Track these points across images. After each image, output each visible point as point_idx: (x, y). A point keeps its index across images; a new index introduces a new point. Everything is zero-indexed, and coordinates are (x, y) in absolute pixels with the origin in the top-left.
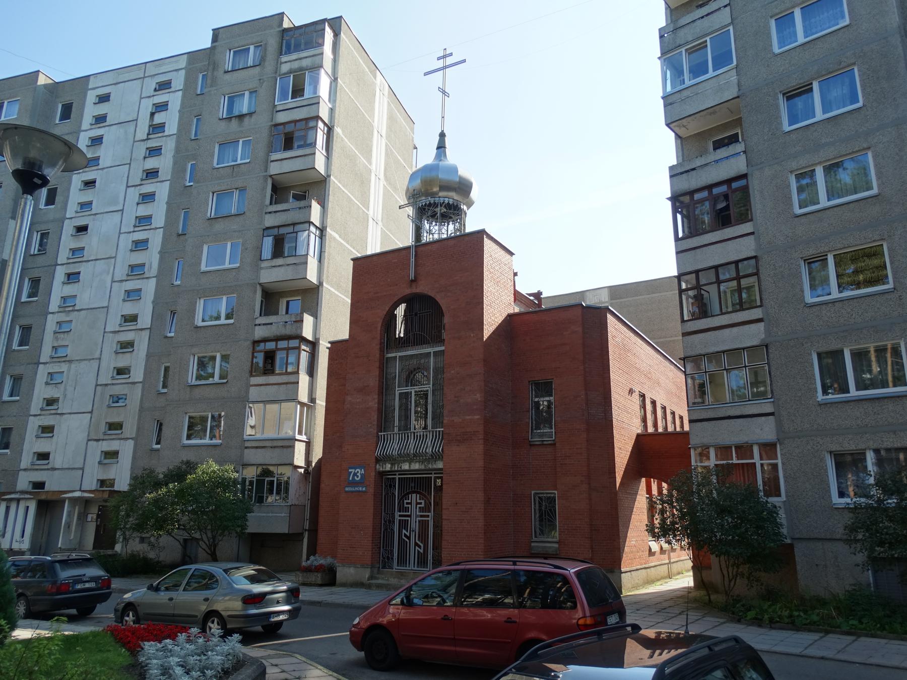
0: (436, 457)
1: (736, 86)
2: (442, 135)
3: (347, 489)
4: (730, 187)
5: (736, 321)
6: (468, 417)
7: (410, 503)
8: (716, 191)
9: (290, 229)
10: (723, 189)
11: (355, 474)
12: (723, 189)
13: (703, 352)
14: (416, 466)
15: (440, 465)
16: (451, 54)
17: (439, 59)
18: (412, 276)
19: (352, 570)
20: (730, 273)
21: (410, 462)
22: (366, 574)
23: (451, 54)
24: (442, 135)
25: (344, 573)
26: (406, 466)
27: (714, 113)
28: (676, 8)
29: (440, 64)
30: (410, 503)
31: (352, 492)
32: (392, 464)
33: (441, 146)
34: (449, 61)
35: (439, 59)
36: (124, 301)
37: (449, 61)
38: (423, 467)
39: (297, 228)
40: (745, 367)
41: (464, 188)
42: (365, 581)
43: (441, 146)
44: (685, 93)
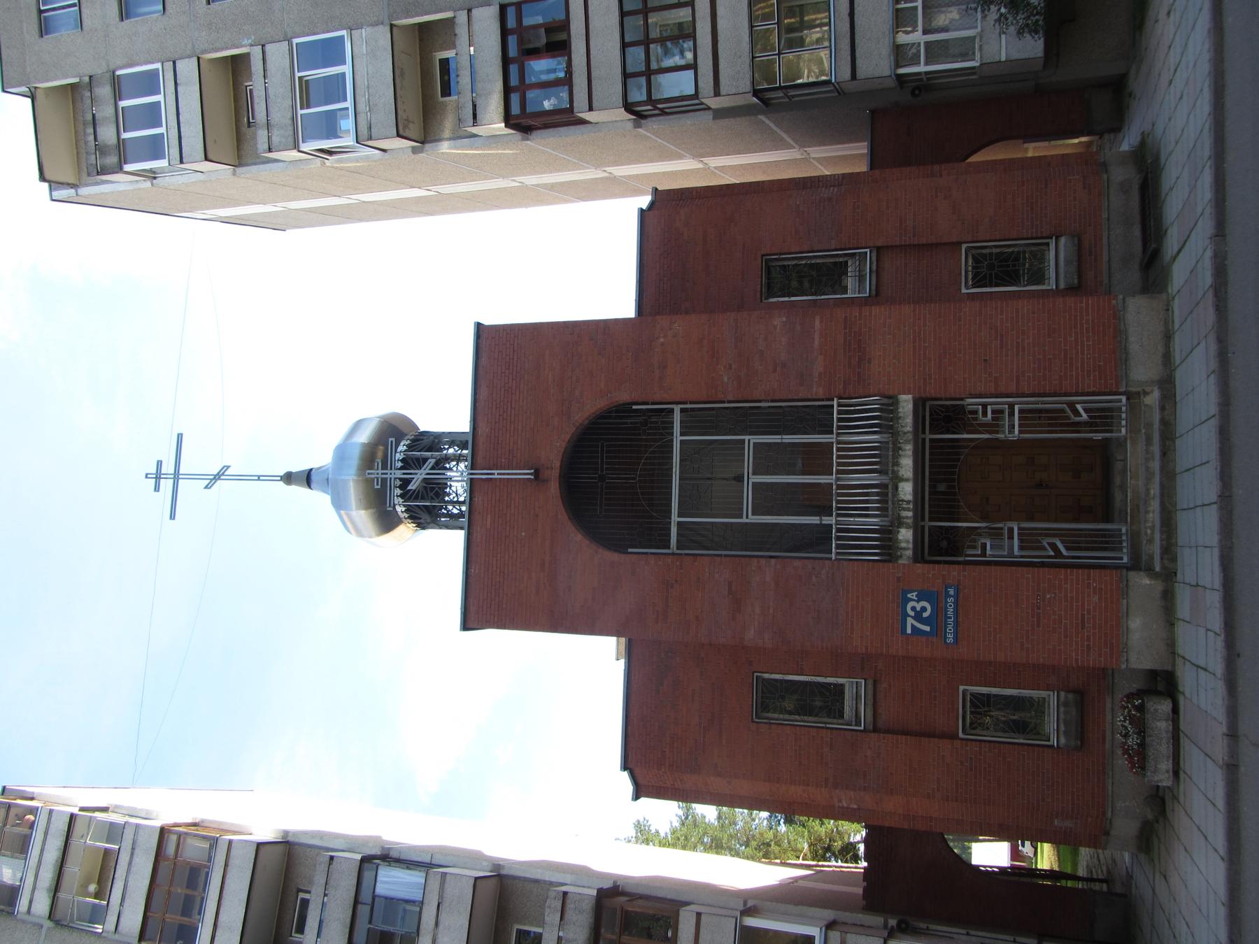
0: (887, 419)
1: (376, 28)
2: (289, 478)
3: (950, 638)
4: (512, 32)
5: (708, 10)
6: (817, 342)
7: (985, 406)
8: (513, 53)
9: (364, 910)
10: (512, 41)
11: (918, 616)
12: (512, 41)
13: (747, 60)
14: (907, 464)
15: (906, 404)
16: (159, 463)
17: (157, 489)
18: (525, 474)
19: (1135, 623)
20: (637, 54)
21: (897, 479)
22: (1142, 581)
23: (159, 463)
24: (289, 478)
25: (1141, 653)
26: (906, 490)
27: (402, 74)
28: (239, 157)
29: (167, 485)
30: (984, 554)
31: (957, 624)
32: (900, 525)
33: (307, 478)
34: (168, 468)
35: (157, 489)
36: (398, 476)
37: (168, 468)
38: (908, 449)
39: (366, 896)
40: (779, 54)
41: (393, 430)
42: (1158, 586)
43: (307, 478)
44: (362, 106)
